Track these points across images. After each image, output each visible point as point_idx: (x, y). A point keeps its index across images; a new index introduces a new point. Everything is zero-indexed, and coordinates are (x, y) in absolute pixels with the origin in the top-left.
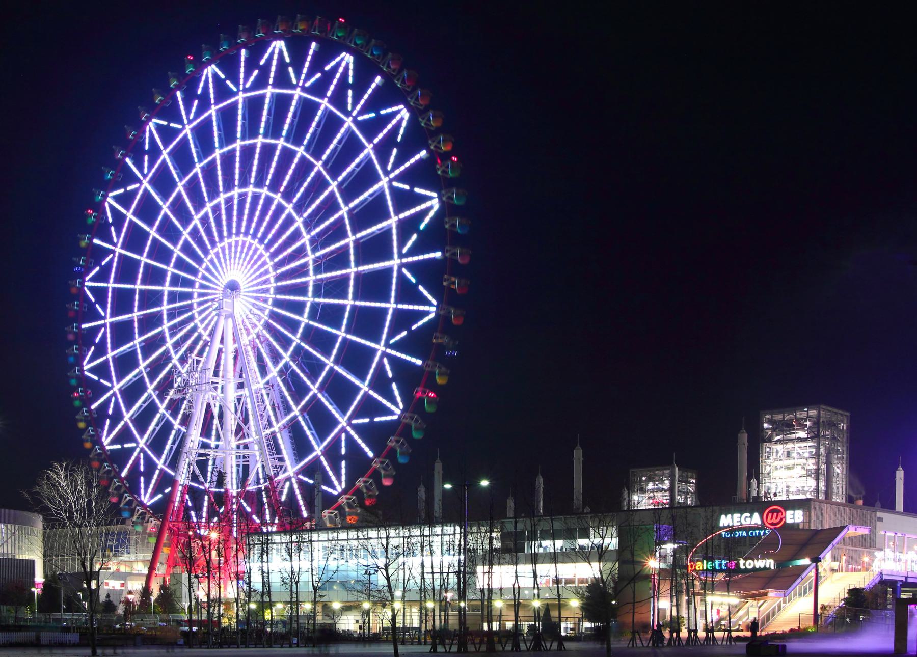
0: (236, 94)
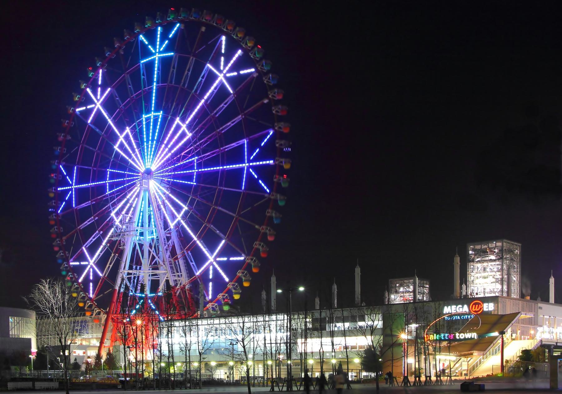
0: (155, 54)
